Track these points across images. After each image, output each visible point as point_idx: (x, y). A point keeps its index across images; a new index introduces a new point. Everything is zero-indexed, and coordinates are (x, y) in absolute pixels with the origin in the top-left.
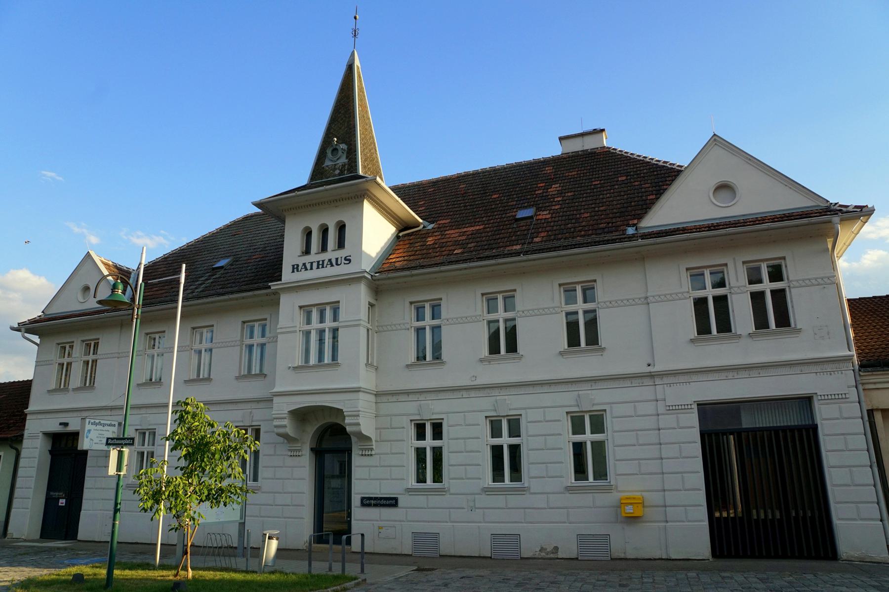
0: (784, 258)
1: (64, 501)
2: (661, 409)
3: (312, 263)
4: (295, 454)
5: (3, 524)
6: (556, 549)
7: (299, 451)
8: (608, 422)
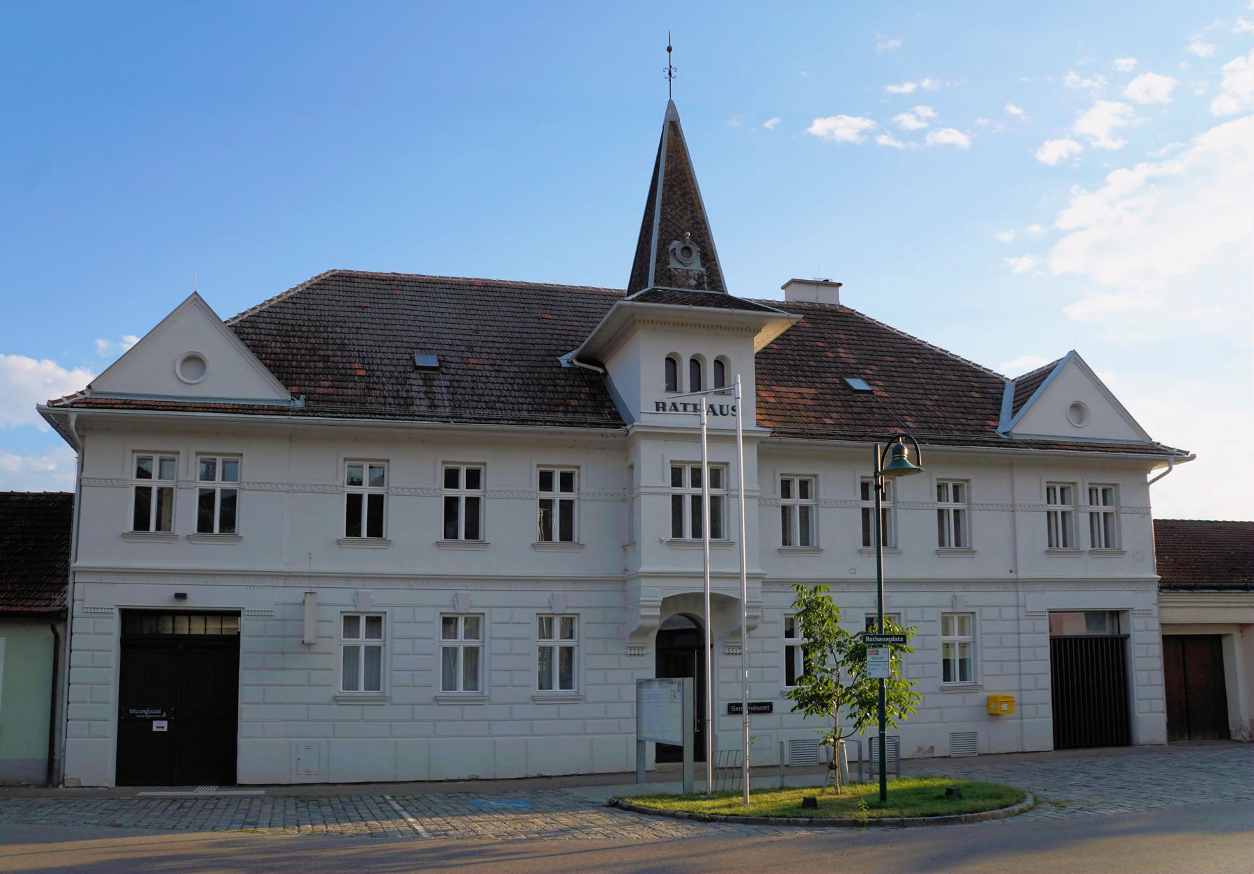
0: (578, 467)
1: (165, 724)
2: (1022, 615)
3: (685, 405)
4: (635, 652)
5: (45, 764)
6: (932, 748)
7: (642, 648)
8: (387, 625)
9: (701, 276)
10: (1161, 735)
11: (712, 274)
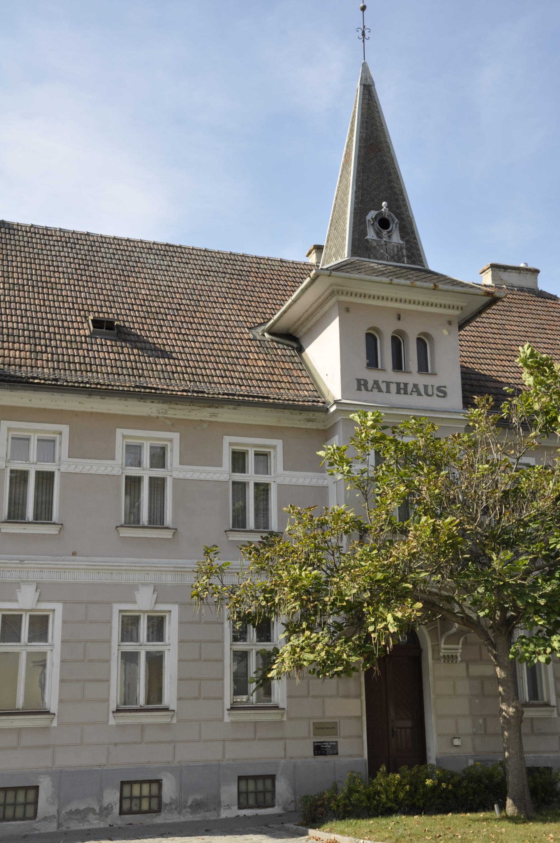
3: (388, 384)
9: (400, 249)
10: (148, 466)
11: (412, 251)
